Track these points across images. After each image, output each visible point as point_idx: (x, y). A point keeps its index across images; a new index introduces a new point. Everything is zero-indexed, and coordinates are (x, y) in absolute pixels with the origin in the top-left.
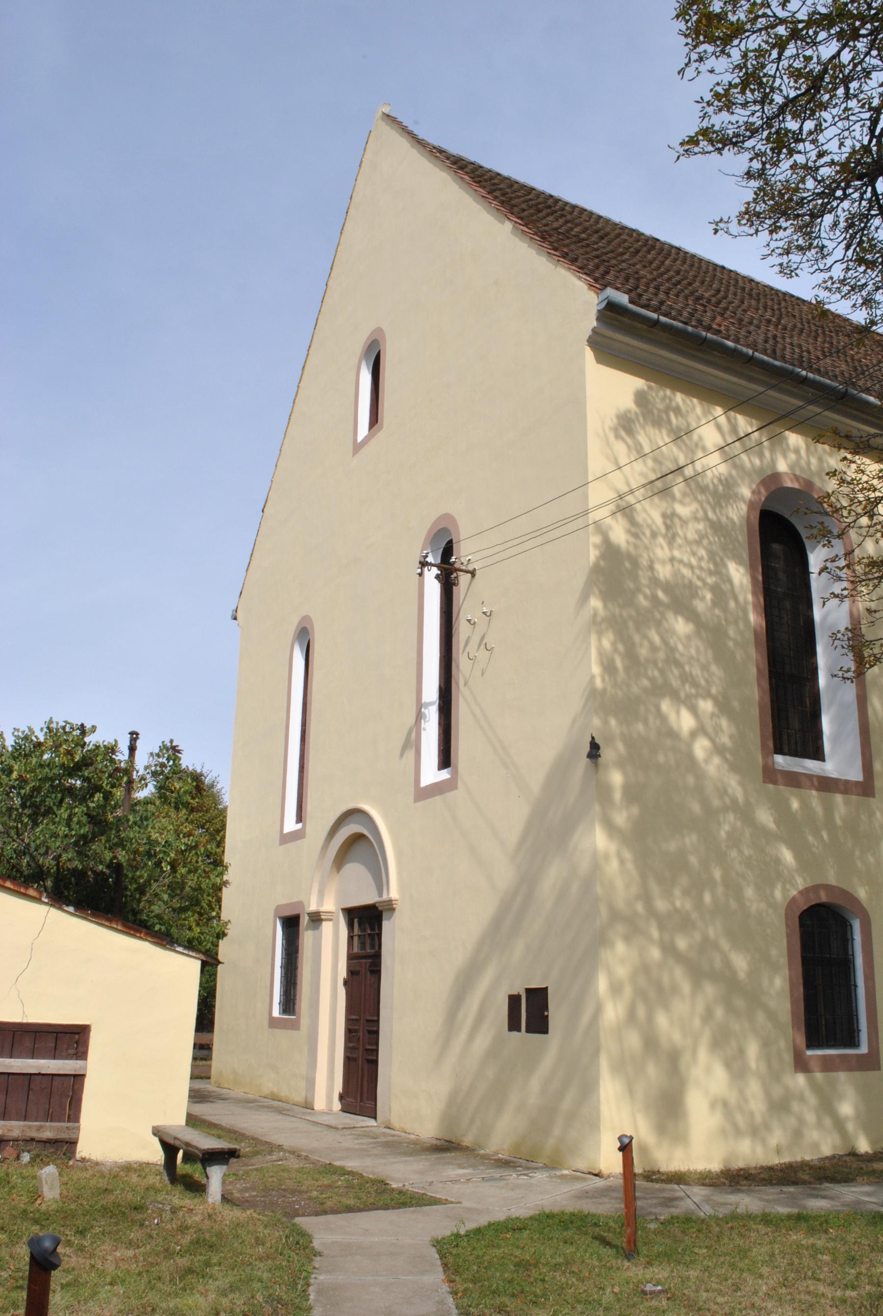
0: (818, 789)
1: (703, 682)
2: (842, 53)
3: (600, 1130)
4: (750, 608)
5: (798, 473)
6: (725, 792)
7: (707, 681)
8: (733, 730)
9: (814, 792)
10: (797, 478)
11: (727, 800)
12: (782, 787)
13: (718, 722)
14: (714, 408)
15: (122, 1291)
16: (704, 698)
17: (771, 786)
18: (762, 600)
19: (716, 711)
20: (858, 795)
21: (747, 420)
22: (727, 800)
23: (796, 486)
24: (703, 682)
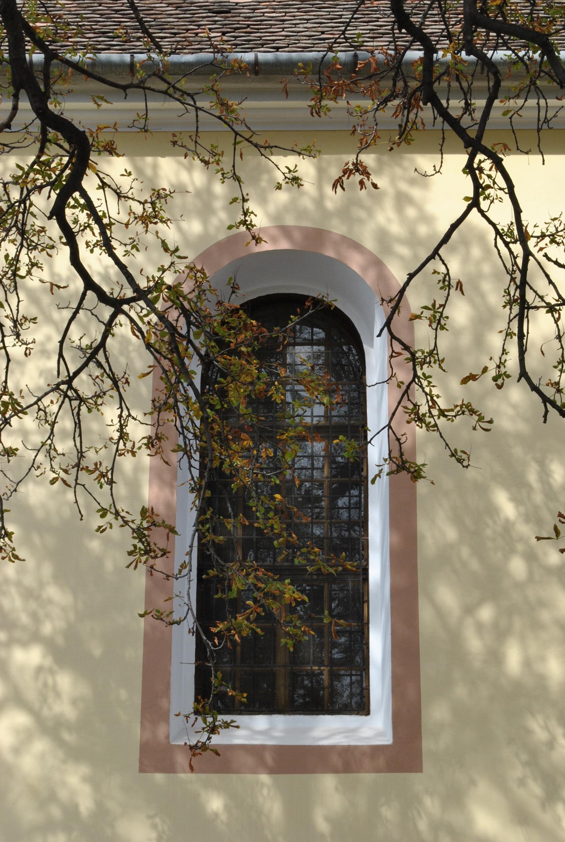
0: (272, 771)
1: (24, 619)
2: (192, 464)
3: (385, 265)
4: (145, 478)
5: (290, 221)
6: (52, 797)
7: (34, 616)
8: (84, 689)
9: (265, 778)
10: (285, 231)
11: (56, 812)
12: (186, 776)
13: (50, 681)
14: (109, 162)
15: (241, 618)
16: (25, 644)
17: (159, 777)
18: (272, 62)
19: (48, 662)
20: (378, 770)
21: (179, 163)
22: (56, 812)
23: (284, 245)
24: (24, 619)
